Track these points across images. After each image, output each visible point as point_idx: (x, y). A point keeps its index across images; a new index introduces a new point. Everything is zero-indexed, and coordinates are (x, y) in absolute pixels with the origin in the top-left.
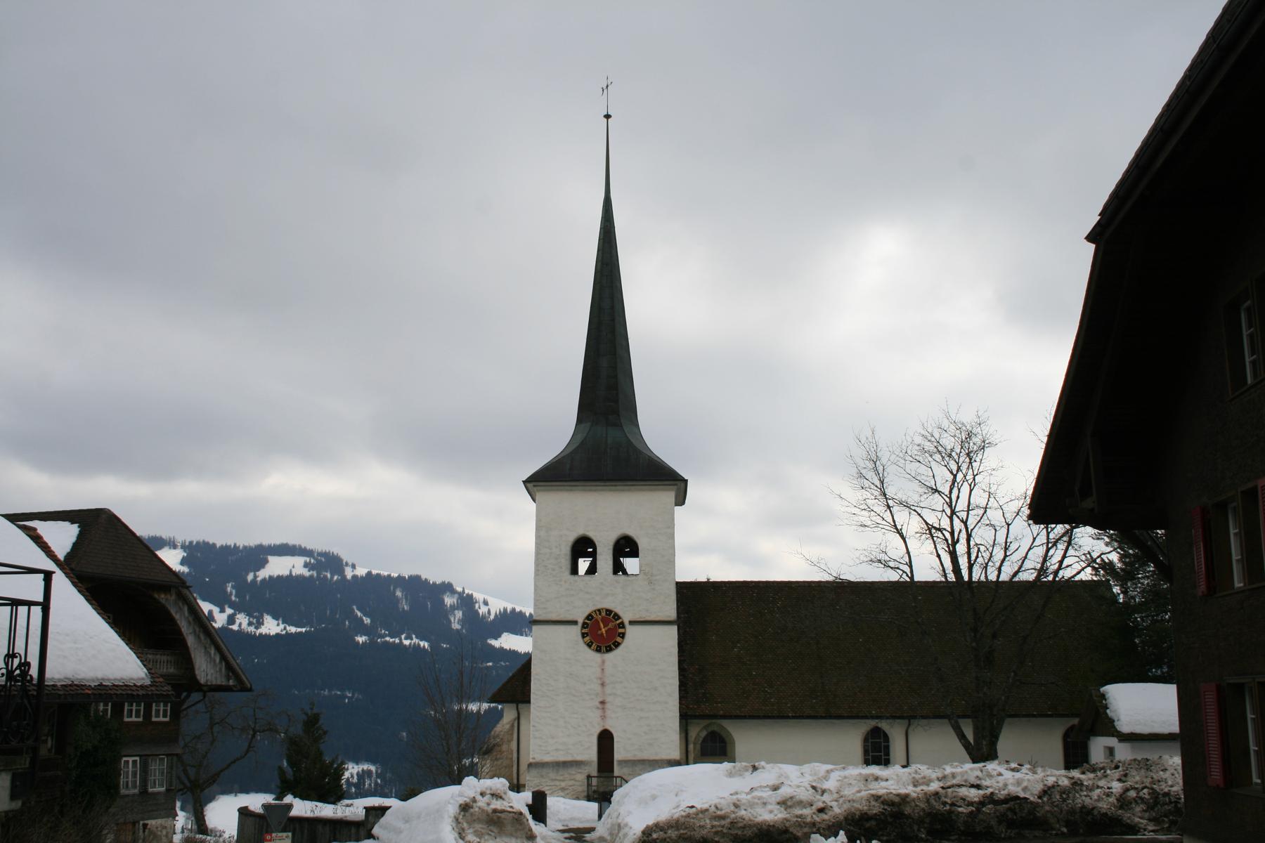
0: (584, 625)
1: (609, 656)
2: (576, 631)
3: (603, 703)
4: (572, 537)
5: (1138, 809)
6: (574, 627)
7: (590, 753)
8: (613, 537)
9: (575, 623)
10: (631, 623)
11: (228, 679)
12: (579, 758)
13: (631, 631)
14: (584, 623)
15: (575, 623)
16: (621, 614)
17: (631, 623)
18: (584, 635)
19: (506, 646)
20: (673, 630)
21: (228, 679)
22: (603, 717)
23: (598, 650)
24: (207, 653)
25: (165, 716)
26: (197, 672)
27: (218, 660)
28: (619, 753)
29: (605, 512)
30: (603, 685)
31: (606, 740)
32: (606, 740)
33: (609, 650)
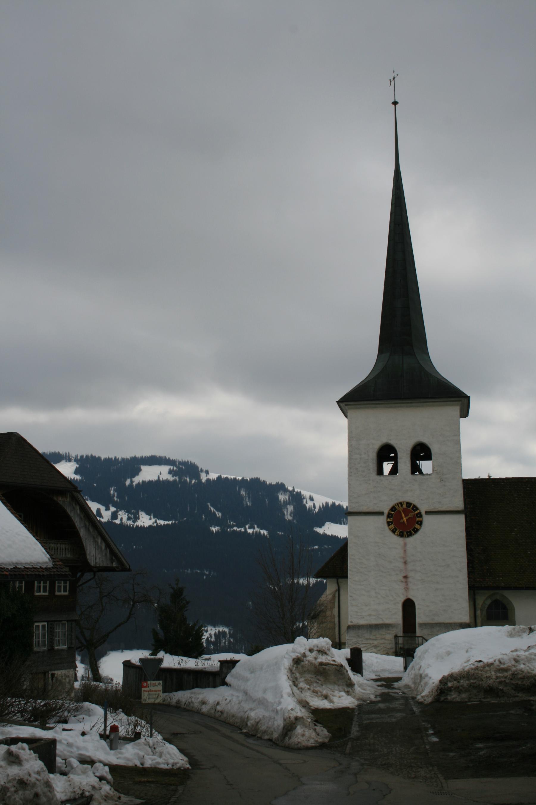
0: (389, 515)
1: (410, 540)
2: (382, 520)
3: (406, 577)
7: (397, 618)
9: (382, 513)
10: (427, 513)
13: (427, 520)
15: (382, 513)
17: (427, 513)
18: (389, 523)
22: (407, 589)
24: (95, 542)
27: (103, 547)
29: (403, 424)
31: (409, 607)
32: (409, 607)
33: (410, 535)
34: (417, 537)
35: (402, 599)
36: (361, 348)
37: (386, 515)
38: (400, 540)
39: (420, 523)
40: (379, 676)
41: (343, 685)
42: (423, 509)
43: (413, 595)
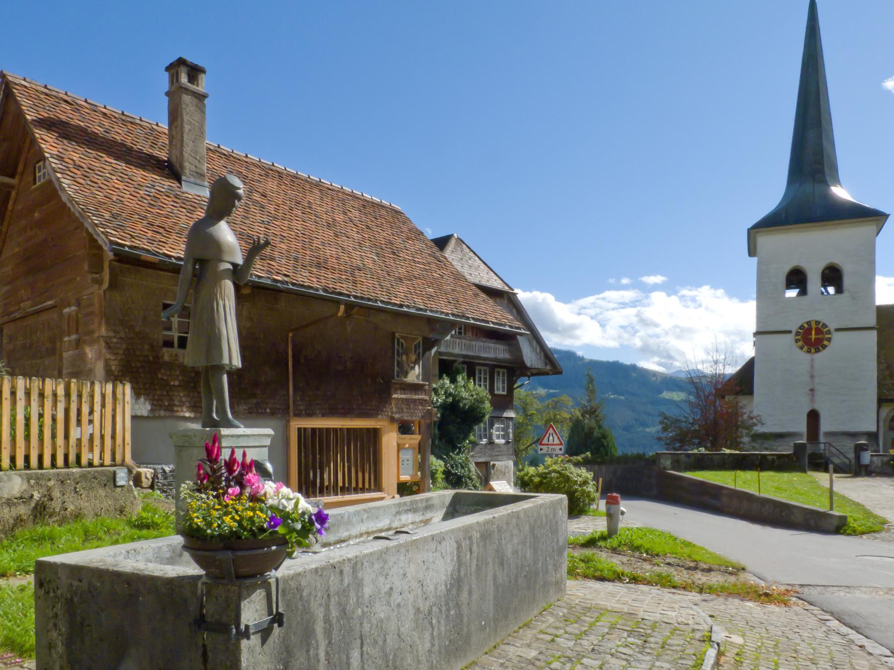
0: (797, 334)
1: (818, 356)
2: (790, 338)
3: (812, 390)
4: (787, 268)
5: (407, 446)
6: (789, 335)
7: (802, 427)
8: (821, 266)
9: (790, 332)
10: (837, 330)
11: (546, 365)
12: (791, 430)
13: (837, 337)
14: (797, 332)
15: (790, 332)
16: (827, 323)
17: (837, 330)
18: (797, 341)
19: (667, 397)
20: (874, 333)
21: (546, 365)
22: (812, 400)
23: (809, 352)
24: (531, 344)
25: (503, 391)
26: (525, 358)
27: (538, 351)
28: (825, 426)
29: (813, 247)
30: (812, 377)
31: (813, 417)
32: (813, 417)
33: (818, 351)
34: (824, 353)
35: (807, 410)
36: (771, 190)
37: (794, 333)
38: (808, 357)
39: (829, 340)
40: (682, 298)
41: (240, 587)
42: (832, 326)
43: (816, 407)
